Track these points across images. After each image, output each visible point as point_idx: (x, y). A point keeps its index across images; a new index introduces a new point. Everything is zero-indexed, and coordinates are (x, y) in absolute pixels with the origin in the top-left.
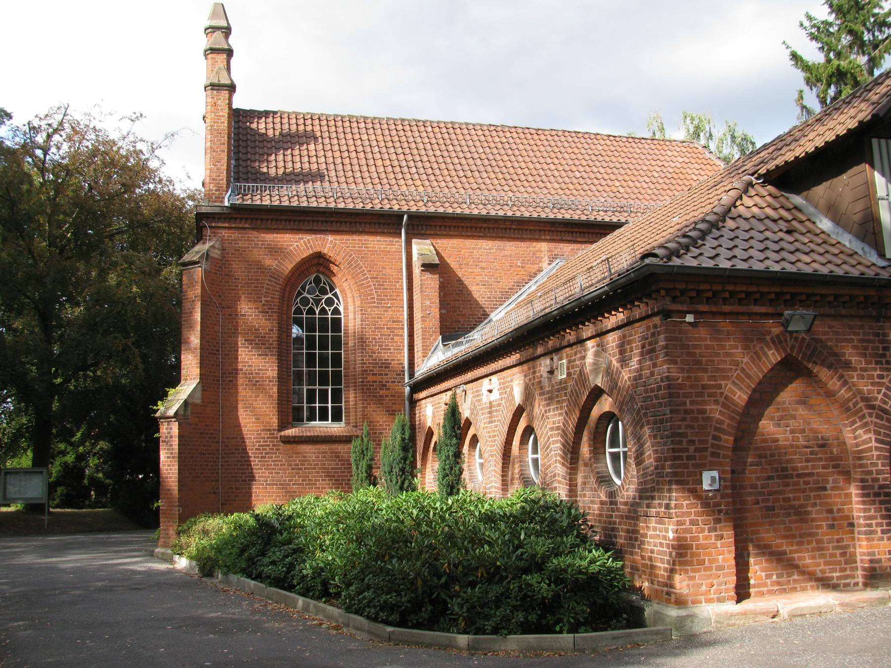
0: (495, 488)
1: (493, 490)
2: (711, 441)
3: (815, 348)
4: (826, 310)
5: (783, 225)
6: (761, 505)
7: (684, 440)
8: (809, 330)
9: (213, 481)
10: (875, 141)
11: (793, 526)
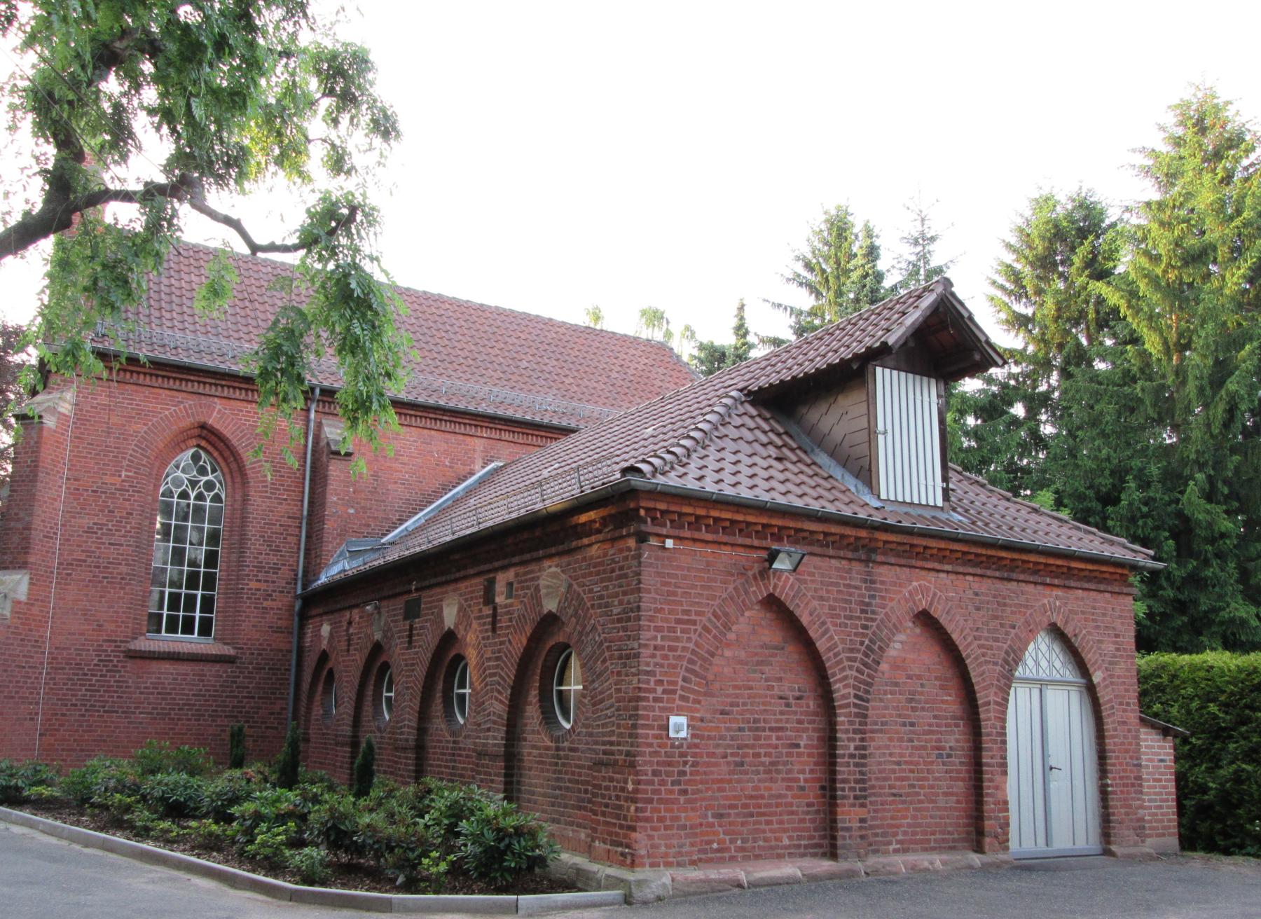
0: (409, 727)
1: (406, 730)
2: (681, 683)
3: (799, 591)
4: (817, 550)
5: (772, 451)
6: (730, 759)
7: (652, 679)
8: (795, 570)
9: (31, 703)
10: (879, 370)
11: (762, 785)
